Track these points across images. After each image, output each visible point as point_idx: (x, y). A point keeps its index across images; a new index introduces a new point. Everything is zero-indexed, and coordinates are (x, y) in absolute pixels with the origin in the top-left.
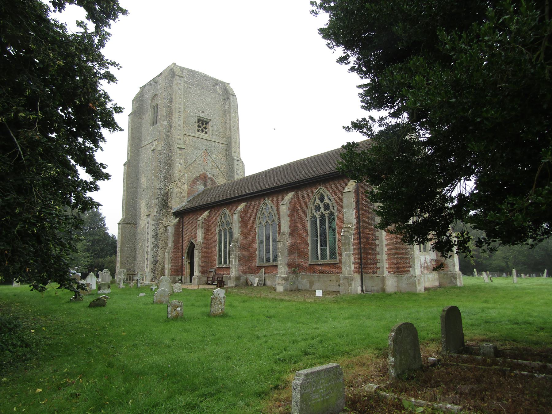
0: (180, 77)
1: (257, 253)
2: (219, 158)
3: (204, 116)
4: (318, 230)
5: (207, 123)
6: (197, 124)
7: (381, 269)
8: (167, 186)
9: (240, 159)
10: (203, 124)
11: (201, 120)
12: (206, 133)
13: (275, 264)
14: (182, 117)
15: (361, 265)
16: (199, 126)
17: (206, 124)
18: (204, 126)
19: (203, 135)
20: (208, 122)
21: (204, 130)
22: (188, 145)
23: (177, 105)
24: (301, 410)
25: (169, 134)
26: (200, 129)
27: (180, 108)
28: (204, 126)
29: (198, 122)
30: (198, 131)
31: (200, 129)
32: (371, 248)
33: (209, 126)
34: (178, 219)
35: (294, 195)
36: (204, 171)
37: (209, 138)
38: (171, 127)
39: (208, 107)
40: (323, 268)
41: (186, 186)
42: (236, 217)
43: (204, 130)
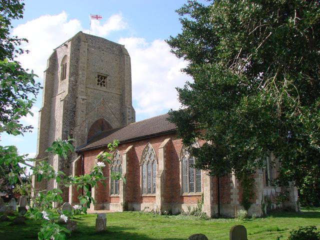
0: (85, 42)
1: (141, 185)
2: (114, 105)
3: (103, 72)
4: (181, 178)
5: (105, 78)
6: (97, 79)
7: (234, 200)
8: (72, 129)
9: (132, 107)
10: (102, 79)
11: (100, 76)
12: (104, 86)
13: (154, 195)
14: (85, 74)
15: (219, 197)
16: (99, 81)
17: (104, 79)
18: (103, 80)
19: (104, 88)
20: (106, 77)
21: (103, 83)
22: (89, 96)
23: (82, 65)
24: (317, 205)
25: (74, 87)
26: (100, 83)
27: (84, 67)
28: (103, 80)
29: (98, 77)
30: (98, 84)
31: (100, 83)
32: (227, 183)
33: (107, 80)
34: (80, 157)
35: (169, 140)
36: (102, 118)
37: (106, 90)
38: (76, 82)
39: (107, 66)
40: (191, 198)
41: (87, 129)
42: (124, 157)
43: (103, 83)
